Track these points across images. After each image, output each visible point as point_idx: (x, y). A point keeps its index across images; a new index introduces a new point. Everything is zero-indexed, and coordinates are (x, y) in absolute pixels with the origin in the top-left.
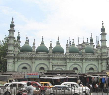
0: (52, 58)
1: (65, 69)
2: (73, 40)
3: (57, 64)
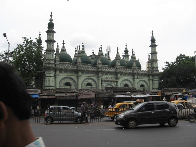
3: (107, 80)
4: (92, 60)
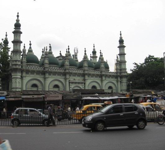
0: (20, 69)
1: (83, 88)
2: (30, 44)
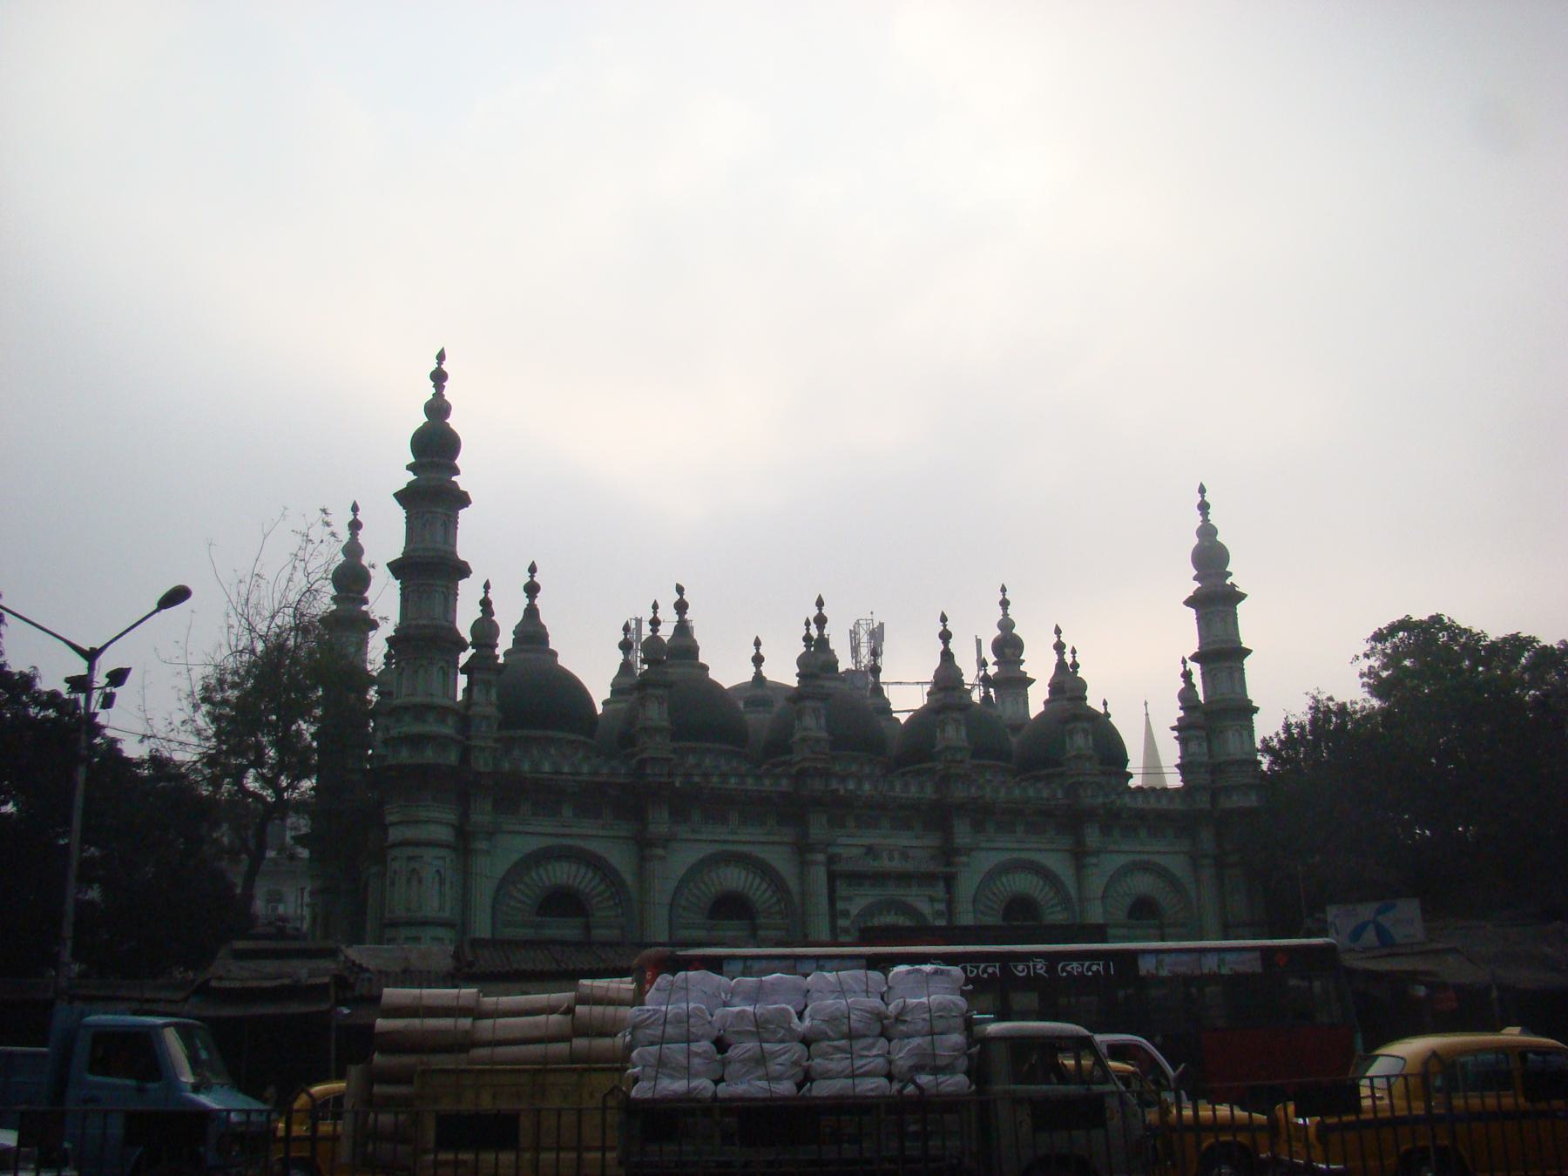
4: (748, 717)
